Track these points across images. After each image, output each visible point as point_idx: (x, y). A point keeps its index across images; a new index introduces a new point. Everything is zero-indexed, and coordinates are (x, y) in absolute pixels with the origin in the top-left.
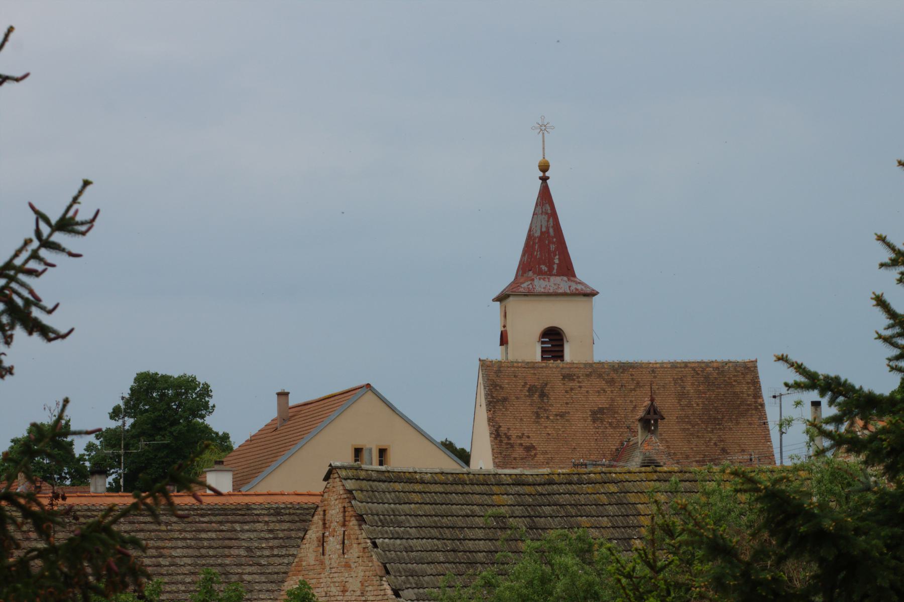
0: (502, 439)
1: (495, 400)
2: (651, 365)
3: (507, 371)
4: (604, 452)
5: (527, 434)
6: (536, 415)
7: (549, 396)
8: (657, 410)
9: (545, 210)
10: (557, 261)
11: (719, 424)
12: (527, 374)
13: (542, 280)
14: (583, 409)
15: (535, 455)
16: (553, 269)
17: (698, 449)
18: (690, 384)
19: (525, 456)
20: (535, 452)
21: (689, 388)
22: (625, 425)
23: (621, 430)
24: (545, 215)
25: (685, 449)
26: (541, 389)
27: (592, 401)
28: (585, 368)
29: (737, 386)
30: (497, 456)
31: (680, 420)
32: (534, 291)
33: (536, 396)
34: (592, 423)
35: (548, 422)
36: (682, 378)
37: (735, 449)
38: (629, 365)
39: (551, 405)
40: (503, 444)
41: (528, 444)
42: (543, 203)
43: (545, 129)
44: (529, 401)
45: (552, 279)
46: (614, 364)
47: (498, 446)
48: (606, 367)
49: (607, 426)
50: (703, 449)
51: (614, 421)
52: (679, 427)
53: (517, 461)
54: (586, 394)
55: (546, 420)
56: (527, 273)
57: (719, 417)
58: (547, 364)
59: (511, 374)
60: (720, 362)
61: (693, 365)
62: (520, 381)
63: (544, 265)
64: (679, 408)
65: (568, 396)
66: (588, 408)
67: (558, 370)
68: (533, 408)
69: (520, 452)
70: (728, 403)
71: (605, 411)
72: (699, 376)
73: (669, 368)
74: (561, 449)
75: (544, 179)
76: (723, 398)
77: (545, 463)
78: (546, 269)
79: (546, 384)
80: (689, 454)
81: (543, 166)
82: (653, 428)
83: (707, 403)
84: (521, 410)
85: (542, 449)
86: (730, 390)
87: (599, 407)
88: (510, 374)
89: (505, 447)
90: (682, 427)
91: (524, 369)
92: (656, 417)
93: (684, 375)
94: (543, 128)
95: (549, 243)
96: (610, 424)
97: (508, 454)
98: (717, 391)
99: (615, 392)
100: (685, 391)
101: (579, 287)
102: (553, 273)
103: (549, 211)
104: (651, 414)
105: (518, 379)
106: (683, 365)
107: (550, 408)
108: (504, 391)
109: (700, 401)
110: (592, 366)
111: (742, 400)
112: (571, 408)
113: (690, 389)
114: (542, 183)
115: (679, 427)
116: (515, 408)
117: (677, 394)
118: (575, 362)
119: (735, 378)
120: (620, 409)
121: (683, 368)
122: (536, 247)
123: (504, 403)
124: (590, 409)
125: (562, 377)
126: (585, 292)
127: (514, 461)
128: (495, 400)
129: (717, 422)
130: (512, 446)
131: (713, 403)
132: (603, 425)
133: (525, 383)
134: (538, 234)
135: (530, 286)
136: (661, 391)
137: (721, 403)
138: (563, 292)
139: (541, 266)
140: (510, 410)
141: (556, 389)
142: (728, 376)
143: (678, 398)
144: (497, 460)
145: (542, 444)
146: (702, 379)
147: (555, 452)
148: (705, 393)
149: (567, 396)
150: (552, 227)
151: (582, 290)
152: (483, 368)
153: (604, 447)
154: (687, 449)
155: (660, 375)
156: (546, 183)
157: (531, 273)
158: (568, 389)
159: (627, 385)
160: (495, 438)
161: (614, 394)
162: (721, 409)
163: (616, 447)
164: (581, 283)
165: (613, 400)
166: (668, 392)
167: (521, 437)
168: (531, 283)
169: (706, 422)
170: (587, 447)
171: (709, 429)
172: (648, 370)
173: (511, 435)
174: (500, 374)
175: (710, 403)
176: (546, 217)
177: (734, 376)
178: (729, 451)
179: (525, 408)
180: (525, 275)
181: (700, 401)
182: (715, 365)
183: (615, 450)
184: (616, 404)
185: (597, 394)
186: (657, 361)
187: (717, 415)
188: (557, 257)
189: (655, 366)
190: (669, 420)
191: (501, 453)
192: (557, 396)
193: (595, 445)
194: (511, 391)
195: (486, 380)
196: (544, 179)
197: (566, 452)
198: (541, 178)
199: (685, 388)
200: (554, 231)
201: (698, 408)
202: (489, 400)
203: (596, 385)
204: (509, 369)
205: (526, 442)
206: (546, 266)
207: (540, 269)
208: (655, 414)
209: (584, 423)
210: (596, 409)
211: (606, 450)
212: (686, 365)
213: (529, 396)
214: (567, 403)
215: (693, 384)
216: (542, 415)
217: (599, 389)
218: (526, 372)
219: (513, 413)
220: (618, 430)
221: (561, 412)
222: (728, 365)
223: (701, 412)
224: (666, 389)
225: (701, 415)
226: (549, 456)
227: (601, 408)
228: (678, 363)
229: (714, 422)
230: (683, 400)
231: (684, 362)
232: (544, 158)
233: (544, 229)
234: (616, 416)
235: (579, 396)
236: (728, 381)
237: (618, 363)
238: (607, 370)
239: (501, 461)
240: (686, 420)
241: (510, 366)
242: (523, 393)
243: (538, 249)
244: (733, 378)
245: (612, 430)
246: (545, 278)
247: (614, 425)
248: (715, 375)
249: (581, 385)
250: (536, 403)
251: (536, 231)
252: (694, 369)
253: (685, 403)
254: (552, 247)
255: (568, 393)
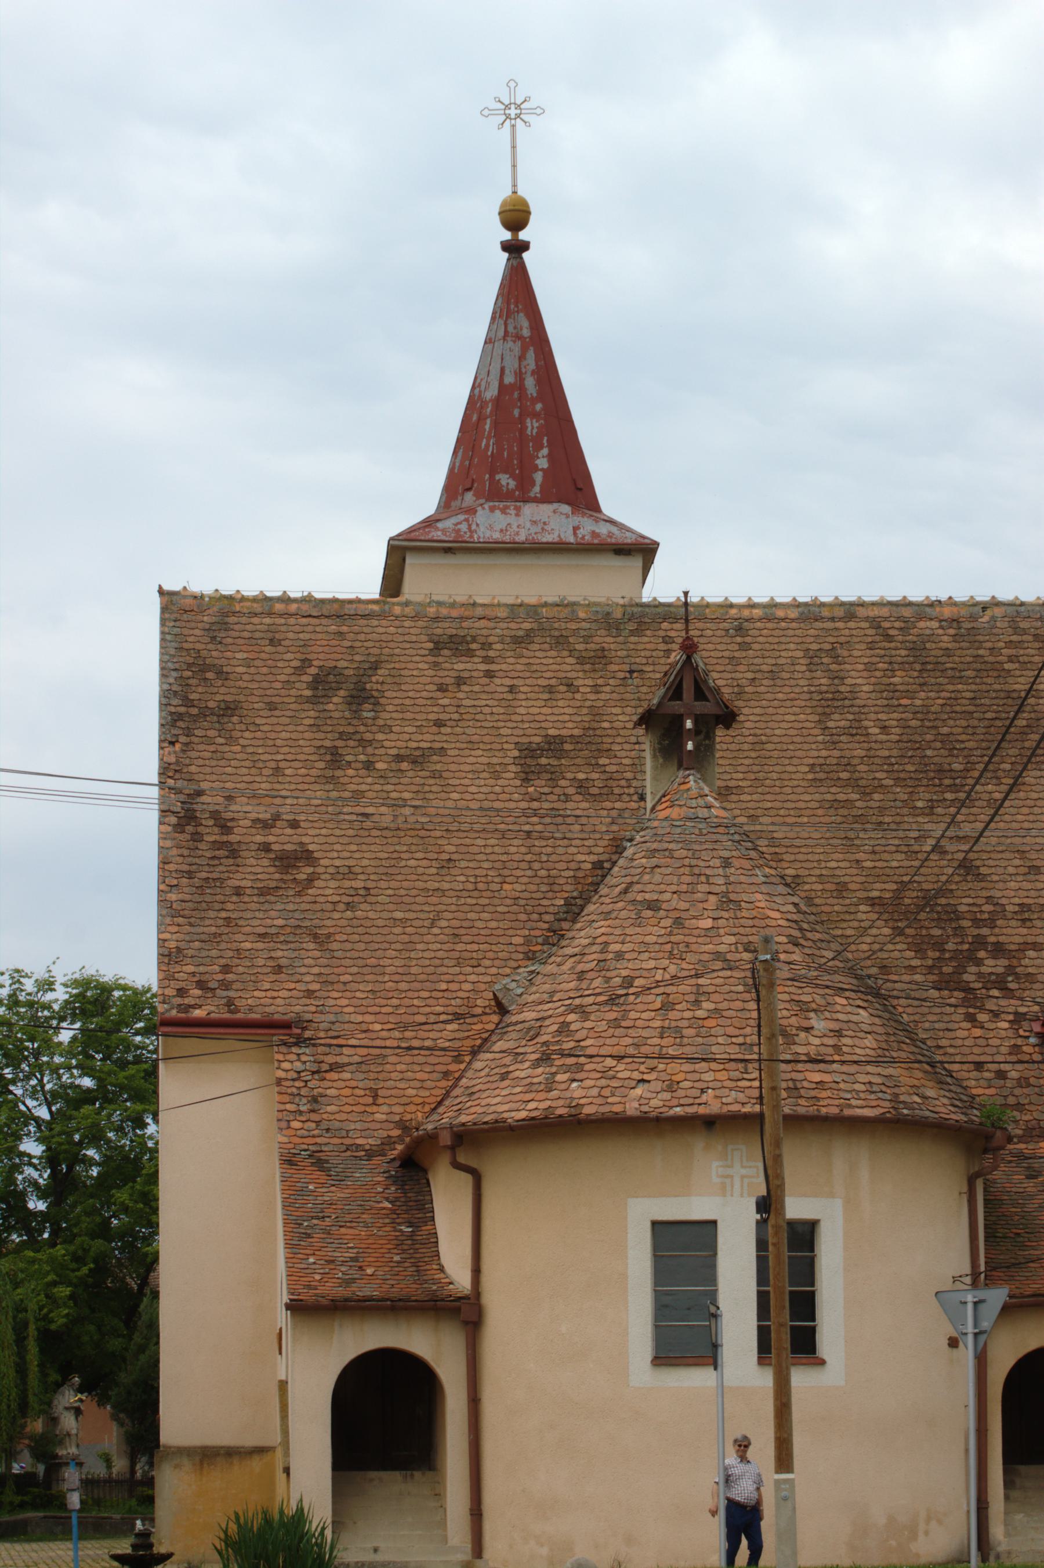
0: (200, 829)
1: (194, 711)
2: (733, 612)
3: (248, 627)
4: (553, 873)
5: (290, 817)
6: (328, 757)
7: (382, 701)
8: (705, 682)
9: (515, 328)
10: (543, 463)
11: (954, 788)
12: (313, 636)
13: (498, 512)
14: (493, 739)
15: (311, 880)
16: (533, 483)
17: (878, 864)
18: (861, 667)
19: (273, 884)
20: (310, 870)
21: (857, 678)
22: (632, 790)
23: (618, 805)
24: (514, 342)
25: (833, 864)
26: (354, 679)
27: (525, 718)
28: (512, 618)
29: (1018, 673)
30: (175, 882)
31: (822, 776)
32: (471, 537)
33: (335, 700)
34: (518, 783)
35: (369, 780)
36: (833, 649)
37: (1006, 863)
38: (659, 610)
39: (387, 728)
40: (202, 846)
41: (289, 847)
42: (508, 308)
43: (518, 116)
44: (312, 713)
45: (529, 510)
46: (607, 609)
47: (186, 852)
48: (582, 615)
49: (571, 791)
50: (895, 864)
51: (595, 776)
52: (817, 797)
53: (246, 899)
54: (510, 696)
55: (363, 772)
56: (460, 498)
57: (956, 766)
58: (387, 607)
59: (262, 635)
60: (964, 604)
61: (875, 612)
62: (289, 656)
63: (506, 472)
64: (820, 738)
65: (446, 702)
66: (509, 739)
67: (420, 624)
68: (321, 735)
69: (259, 870)
70: (986, 723)
71: (567, 747)
72: (893, 645)
73: (793, 620)
74: (403, 863)
75: (515, 249)
76: (971, 708)
77: (341, 907)
78: (512, 484)
79: (375, 666)
80: (847, 879)
81: (510, 211)
82: (690, 746)
83: (914, 723)
84: (279, 742)
85: (337, 863)
86: (997, 687)
87: (547, 735)
88: (257, 635)
89: (208, 854)
90: (828, 797)
91: (305, 621)
92: (701, 707)
93: (842, 639)
94: (513, 112)
95: (520, 414)
96: (582, 787)
97: (215, 875)
98: (951, 687)
99: (607, 689)
100: (842, 689)
101: (603, 529)
102: (532, 494)
103: (526, 333)
104: (685, 696)
105: (280, 649)
106: (839, 612)
107: (380, 736)
108: (228, 683)
109: (892, 719)
110: (536, 613)
111: (1033, 715)
112: (452, 738)
113: (859, 681)
114: (508, 260)
115: (817, 797)
116: (259, 734)
117: (817, 697)
118: (480, 600)
119: (1013, 652)
120: (619, 740)
121: (840, 619)
122: (487, 427)
123: (226, 719)
124: (517, 740)
125: (431, 645)
126: (620, 541)
127: (234, 898)
128: (194, 711)
129: (947, 782)
130: (234, 853)
131: (939, 723)
132: (557, 790)
133: (303, 661)
134: (492, 392)
135: (464, 527)
136: (762, 689)
137: (964, 723)
138: (556, 540)
139: (497, 477)
140: (242, 741)
141: (408, 680)
142: (989, 645)
143: (820, 710)
144: (173, 897)
145: (337, 847)
146: (903, 653)
147: (381, 870)
148: (910, 694)
149: (441, 702)
150: (533, 373)
151: (611, 537)
152: (167, 616)
153: (553, 858)
154: (842, 864)
155: (761, 639)
156: (522, 258)
157: (469, 497)
158: (448, 681)
159: (650, 668)
160: (179, 828)
161: (603, 696)
162: (963, 742)
163: (593, 858)
164: (612, 522)
165: (596, 714)
166: (787, 689)
167: (267, 825)
168: (467, 520)
169: (910, 783)
170: (492, 857)
171: (920, 804)
172: (726, 625)
173: (233, 819)
174: (223, 634)
175: (927, 724)
176: (517, 348)
177: (1009, 644)
178: (983, 870)
179: (294, 736)
180: (453, 504)
181: (892, 719)
182: (947, 613)
183: (589, 866)
184: (606, 725)
185: (546, 696)
186: (756, 600)
187: (949, 759)
188: (545, 451)
189: (746, 613)
190: (785, 776)
191: (190, 875)
192: (407, 702)
193: (523, 850)
194: (255, 685)
195: (172, 651)
196: (515, 249)
197: (420, 870)
198: (506, 247)
199: (843, 678)
200: (539, 382)
201: (884, 737)
202: (173, 709)
203: (545, 668)
204: (256, 620)
205: (283, 839)
206: (513, 476)
207: (495, 484)
208: (697, 699)
209: (492, 782)
210: (538, 739)
211: (562, 866)
212: (850, 611)
213: (313, 700)
214: (439, 724)
215: (870, 667)
216: (349, 758)
217: (553, 682)
218: (310, 628)
219: (250, 750)
220: (608, 805)
221: (418, 748)
222: (989, 612)
223: (895, 753)
224: (779, 682)
225: (893, 760)
226: (359, 884)
227: (554, 737)
228: (823, 605)
229: (937, 781)
230: (836, 717)
231: (843, 604)
232: (515, 192)
233: (509, 379)
234: (602, 761)
235: (484, 703)
236: (991, 659)
237: (623, 606)
238: (584, 625)
239: (188, 897)
240: (844, 775)
241: (259, 610)
242: (293, 692)
243: (490, 432)
244: (1004, 651)
245: (585, 805)
246: (507, 507)
247: (594, 791)
248: (946, 642)
249: (493, 667)
250: (335, 722)
251: (488, 383)
252: (875, 623)
253: (843, 723)
254: (532, 426)
255: (446, 691)
